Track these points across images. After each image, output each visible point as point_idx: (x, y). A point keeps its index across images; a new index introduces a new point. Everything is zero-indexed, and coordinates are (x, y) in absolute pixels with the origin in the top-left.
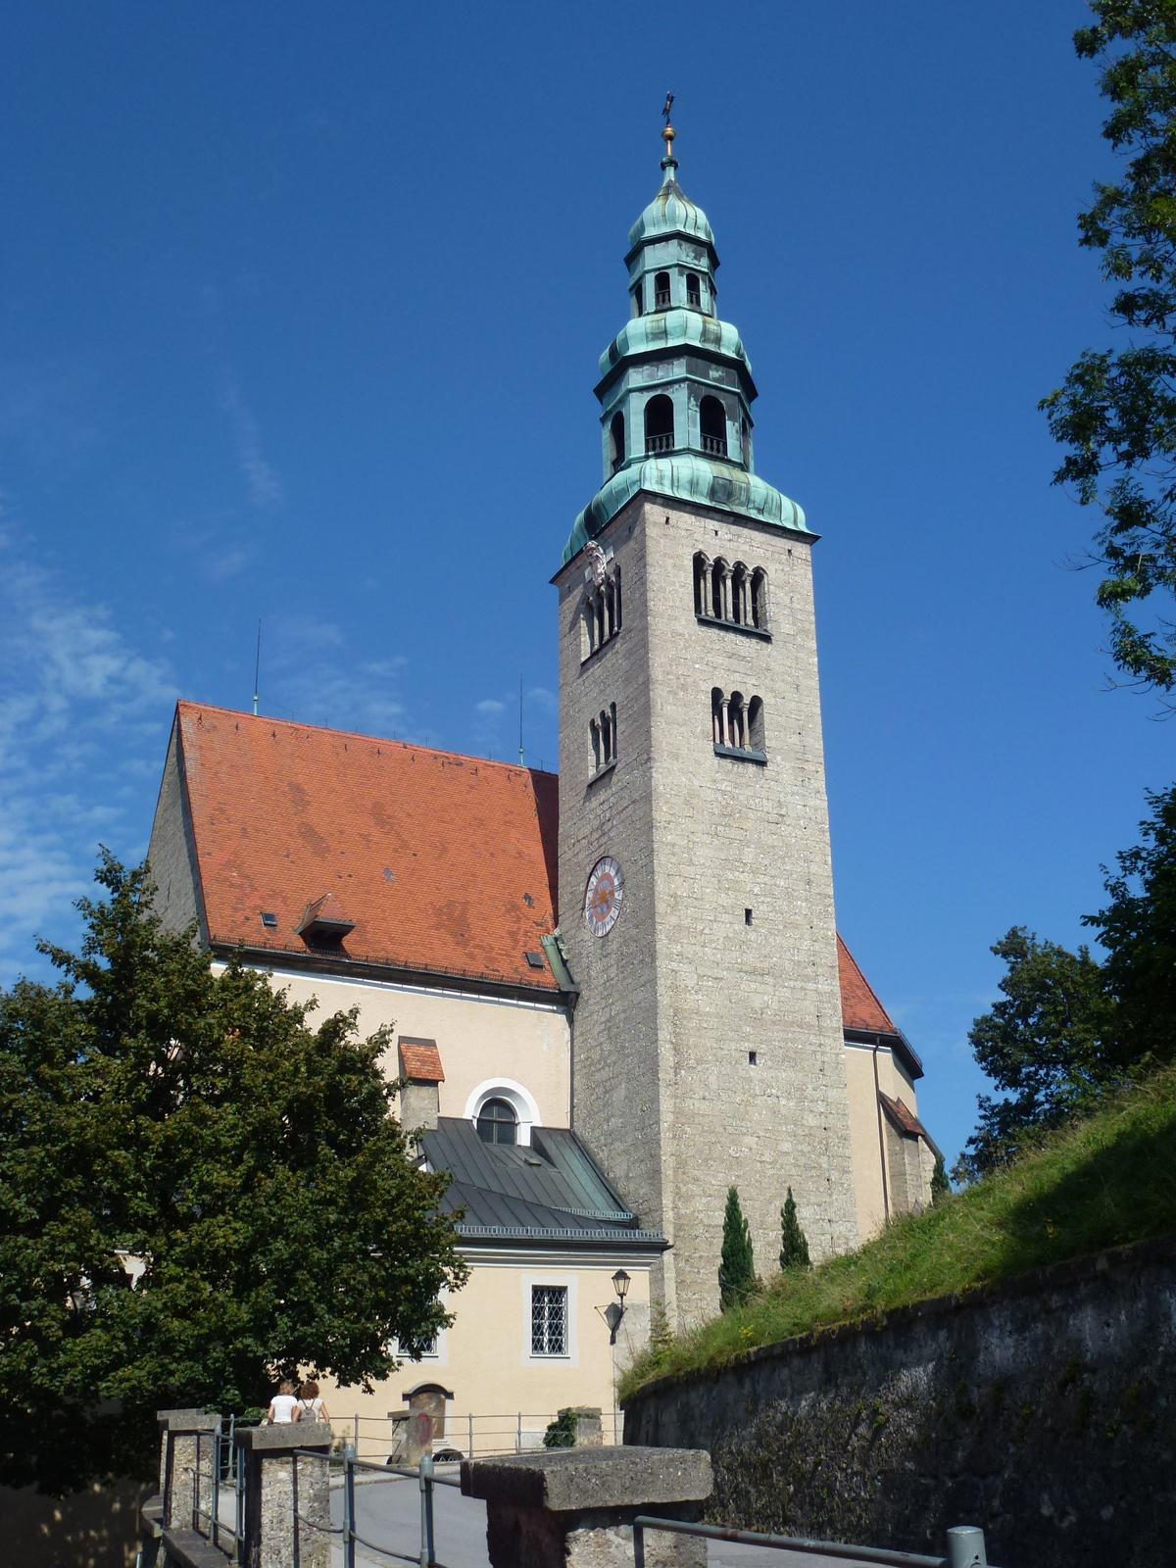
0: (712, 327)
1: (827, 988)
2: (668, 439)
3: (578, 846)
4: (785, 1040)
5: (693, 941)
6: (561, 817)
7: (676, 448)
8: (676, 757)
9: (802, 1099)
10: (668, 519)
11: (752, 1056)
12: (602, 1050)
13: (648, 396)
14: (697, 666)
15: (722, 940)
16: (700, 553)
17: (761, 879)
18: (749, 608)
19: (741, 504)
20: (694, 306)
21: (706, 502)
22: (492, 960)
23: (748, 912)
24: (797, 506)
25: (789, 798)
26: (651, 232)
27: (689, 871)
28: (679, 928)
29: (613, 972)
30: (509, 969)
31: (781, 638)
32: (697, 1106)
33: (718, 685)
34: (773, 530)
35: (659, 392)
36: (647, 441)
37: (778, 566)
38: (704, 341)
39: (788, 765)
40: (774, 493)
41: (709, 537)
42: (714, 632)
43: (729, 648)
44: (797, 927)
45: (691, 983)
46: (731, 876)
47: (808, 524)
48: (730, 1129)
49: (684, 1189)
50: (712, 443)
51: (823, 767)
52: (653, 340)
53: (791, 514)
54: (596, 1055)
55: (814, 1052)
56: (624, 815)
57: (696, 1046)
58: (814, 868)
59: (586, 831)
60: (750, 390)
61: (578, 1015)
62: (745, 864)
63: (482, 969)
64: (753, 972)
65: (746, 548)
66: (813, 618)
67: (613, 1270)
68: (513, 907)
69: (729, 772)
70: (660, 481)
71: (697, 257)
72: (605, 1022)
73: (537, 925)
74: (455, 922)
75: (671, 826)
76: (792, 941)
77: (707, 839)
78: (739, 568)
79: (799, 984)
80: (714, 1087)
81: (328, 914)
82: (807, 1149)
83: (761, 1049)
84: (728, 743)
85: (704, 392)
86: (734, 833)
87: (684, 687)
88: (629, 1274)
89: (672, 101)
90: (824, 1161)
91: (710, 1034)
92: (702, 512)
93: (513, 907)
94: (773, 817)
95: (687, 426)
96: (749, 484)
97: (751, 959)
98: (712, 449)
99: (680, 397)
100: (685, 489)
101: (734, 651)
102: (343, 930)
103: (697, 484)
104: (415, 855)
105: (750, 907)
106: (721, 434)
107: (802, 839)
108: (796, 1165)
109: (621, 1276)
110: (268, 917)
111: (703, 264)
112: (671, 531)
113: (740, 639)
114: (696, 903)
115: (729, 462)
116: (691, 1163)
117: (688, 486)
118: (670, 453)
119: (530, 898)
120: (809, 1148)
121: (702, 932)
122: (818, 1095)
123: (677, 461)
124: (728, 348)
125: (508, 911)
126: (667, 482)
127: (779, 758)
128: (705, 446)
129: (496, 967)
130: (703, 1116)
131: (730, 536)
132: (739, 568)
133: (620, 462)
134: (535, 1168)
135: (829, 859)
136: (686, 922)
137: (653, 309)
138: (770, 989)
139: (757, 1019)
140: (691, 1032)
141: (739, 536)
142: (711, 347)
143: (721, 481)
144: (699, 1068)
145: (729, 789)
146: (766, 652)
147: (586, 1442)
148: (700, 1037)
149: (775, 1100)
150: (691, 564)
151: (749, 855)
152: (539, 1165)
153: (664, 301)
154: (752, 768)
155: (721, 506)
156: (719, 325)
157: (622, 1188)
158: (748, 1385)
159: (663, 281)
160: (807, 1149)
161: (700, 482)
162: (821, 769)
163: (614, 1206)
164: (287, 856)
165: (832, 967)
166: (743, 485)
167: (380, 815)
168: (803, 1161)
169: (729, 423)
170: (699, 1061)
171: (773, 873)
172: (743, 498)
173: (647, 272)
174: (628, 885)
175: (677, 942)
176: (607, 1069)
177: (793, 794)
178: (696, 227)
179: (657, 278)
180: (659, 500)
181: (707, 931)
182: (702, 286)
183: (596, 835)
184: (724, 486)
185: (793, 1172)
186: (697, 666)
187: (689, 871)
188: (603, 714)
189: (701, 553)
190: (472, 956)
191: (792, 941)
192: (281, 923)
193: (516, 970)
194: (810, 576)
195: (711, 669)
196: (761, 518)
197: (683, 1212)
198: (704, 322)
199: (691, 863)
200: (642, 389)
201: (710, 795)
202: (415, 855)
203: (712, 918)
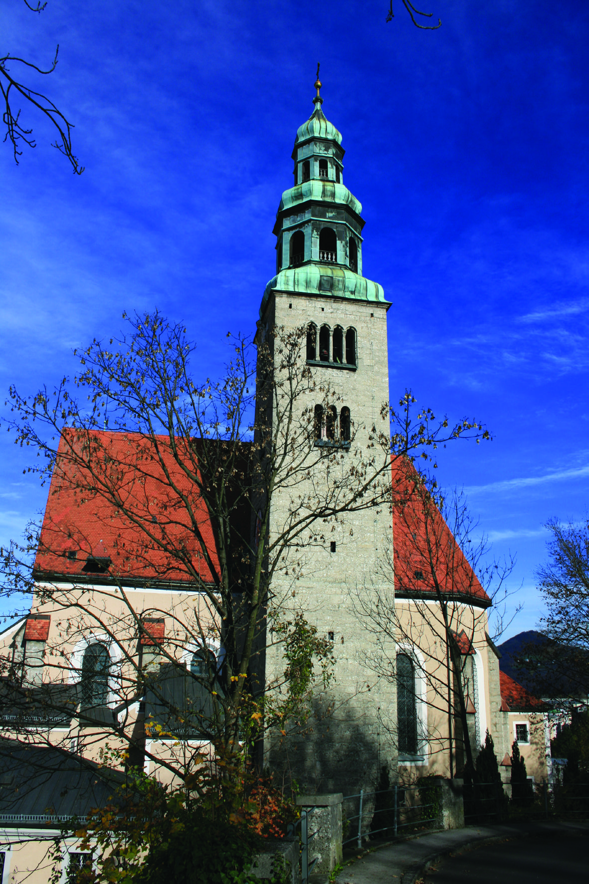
21: (317, 292)
26: (302, 139)
44: (366, 549)
47: (385, 297)
53: (374, 290)
65: (343, 316)
70: (287, 283)
71: (327, 149)
78: (338, 329)
95: (313, 248)
97: (333, 573)
102: (107, 563)
106: (334, 250)
112: (293, 312)
117: (304, 284)
126: (291, 283)
132: (338, 329)
142: (328, 199)
146: (352, 379)
147: (369, 790)
149: (344, 661)
155: (327, 291)
169: (338, 242)
172: (341, 286)
189: (325, 324)
191: (362, 559)
198: (324, 186)
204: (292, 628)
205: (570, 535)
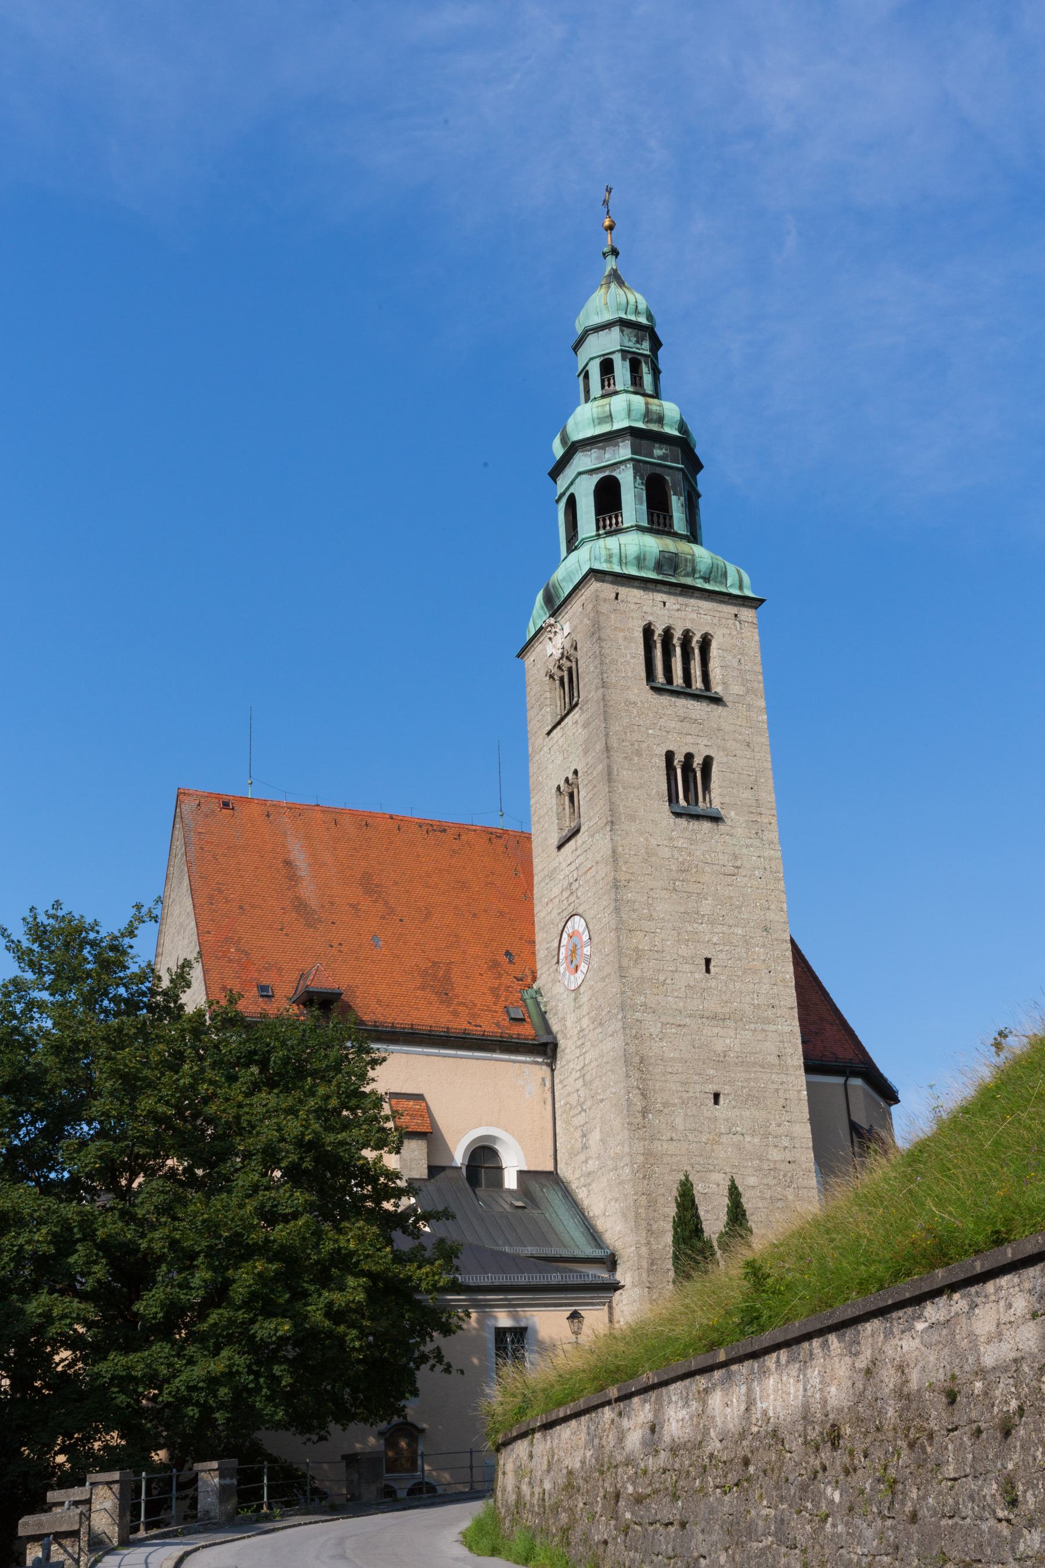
0: (654, 408)
1: (787, 1029)
2: (617, 518)
3: (550, 905)
4: (748, 1080)
5: (655, 991)
6: (535, 878)
7: (625, 526)
8: (632, 818)
9: (765, 1136)
10: (617, 594)
11: (716, 1097)
12: (579, 1096)
13: (596, 478)
14: (650, 732)
15: (683, 989)
16: (650, 624)
17: (719, 929)
18: (699, 673)
19: (687, 575)
20: (638, 389)
21: (653, 575)
22: (474, 1016)
23: (708, 961)
24: (743, 572)
25: (744, 851)
27: (647, 925)
28: (642, 980)
29: (585, 1022)
30: (488, 1026)
31: (731, 699)
32: (665, 1147)
33: (671, 748)
34: (718, 597)
35: (607, 473)
36: (597, 521)
37: (726, 631)
38: (647, 422)
39: (742, 819)
40: (720, 560)
41: (658, 608)
42: (665, 700)
43: (681, 713)
45: (655, 1030)
46: (690, 928)
48: (698, 1167)
49: (655, 1227)
50: (658, 517)
51: (775, 818)
52: (599, 424)
54: (573, 1100)
55: (777, 1090)
56: (590, 874)
57: (662, 1090)
58: (771, 916)
59: (556, 891)
60: (694, 465)
61: (559, 1064)
62: (703, 916)
63: (465, 1026)
64: (715, 1017)
65: (694, 616)
66: (761, 677)
67: (567, 1312)
68: (495, 965)
69: (686, 829)
72: (580, 1070)
73: (518, 980)
74: (439, 983)
75: (632, 884)
76: (751, 986)
77: (665, 894)
79: (759, 1026)
80: (681, 1127)
81: (324, 982)
82: (772, 1182)
83: (725, 1090)
84: (682, 802)
85: (649, 470)
86: (693, 888)
87: (638, 753)
88: (583, 1313)
89: (610, 192)
90: (790, 1193)
91: (675, 1078)
92: (650, 586)
93: (495, 965)
94: (730, 869)
95: (632, 505)
96: (693, 555)
97: (712, 1005)
98: (659, 525)
99: (626, 477)
100: (632, 565)
101: (686, 715)
103: (644, 559)
104: (401, 920)
105: (709, 956)
107: (758, 888)
108: (763, 1198)
109: (575, 1316)
110: (263, 988)
111: (645, 348)
112: (622, 607)
113: (691, 703)
114: (657, 956)
115: (675, 535)
116: (661, 1200)
117: (635, 562)
118: (618, 531)
119: (511, 954)
120: (775, 1182)
121: (664, 983)
122: (780, 1131)
123: (623, 538)
124: (671, 426)
125: (490, 968)
126: (615, 560)
127: (732, 813)
128: (651, 521)
129: (478, 1022)
130: (671, 1156)
131: (677, 607)
133: (572, 544)
134: (520, 1211)
135: (785, 906)
136: (648, 974)
137: (599, 393)
138: (732, 1033)
139: (721, 1061)
140: (657, 1077)
141: (686, 605)
142: (654, 427)
143: (666, 555)
144: (666, 1111)
145: (685, 845)
146: (716, 714)
148: (666, 1081)
149: (740, 1138)
150: (641, 635)
151: (706, 906)
152: (524, 1208)
153: (609, 385)
154: (706, 825)
156: (661, 406)
157: (601, 1224)
158: (549, 1442)
159: (607, 367)
160: (772, 1182)
161: (648, 557)
162: (774, 821)
163: (593, 1243)
164: (282, 930)
165: (792, 1008)
166: (689, 557)
167: (369, 885)
168: (768, 1194)
170: (665, 1105)
171: (731, 922)
172: (689, 569)
173: (592, 359)
174: (595, 939)
175: (640, 993)
176: (583, 1114)
177: (747, 846)
178: (637, 312)
179: (602, 364)
180: (608, 578)
181: (668, 981)
182: (645, 369)
183: (566, 894)
184: (670, 559)
185: (760, 1205)
186: (650, 732)
187: (647, 925)
188: (567, 780)
190: (455, 1014)
192: (279, 993)
193: (498, 1025)
194: (757, 638)
195: (665, 734)
196: (707, 586)
197: (655, 1247)
198: (647, 404)
199: (651, 918)
200: (591, 472)
201: (665, 852)
202: (401, 920)
203: (673, 969)
204: (391, 1256)
205: (488, 1414)
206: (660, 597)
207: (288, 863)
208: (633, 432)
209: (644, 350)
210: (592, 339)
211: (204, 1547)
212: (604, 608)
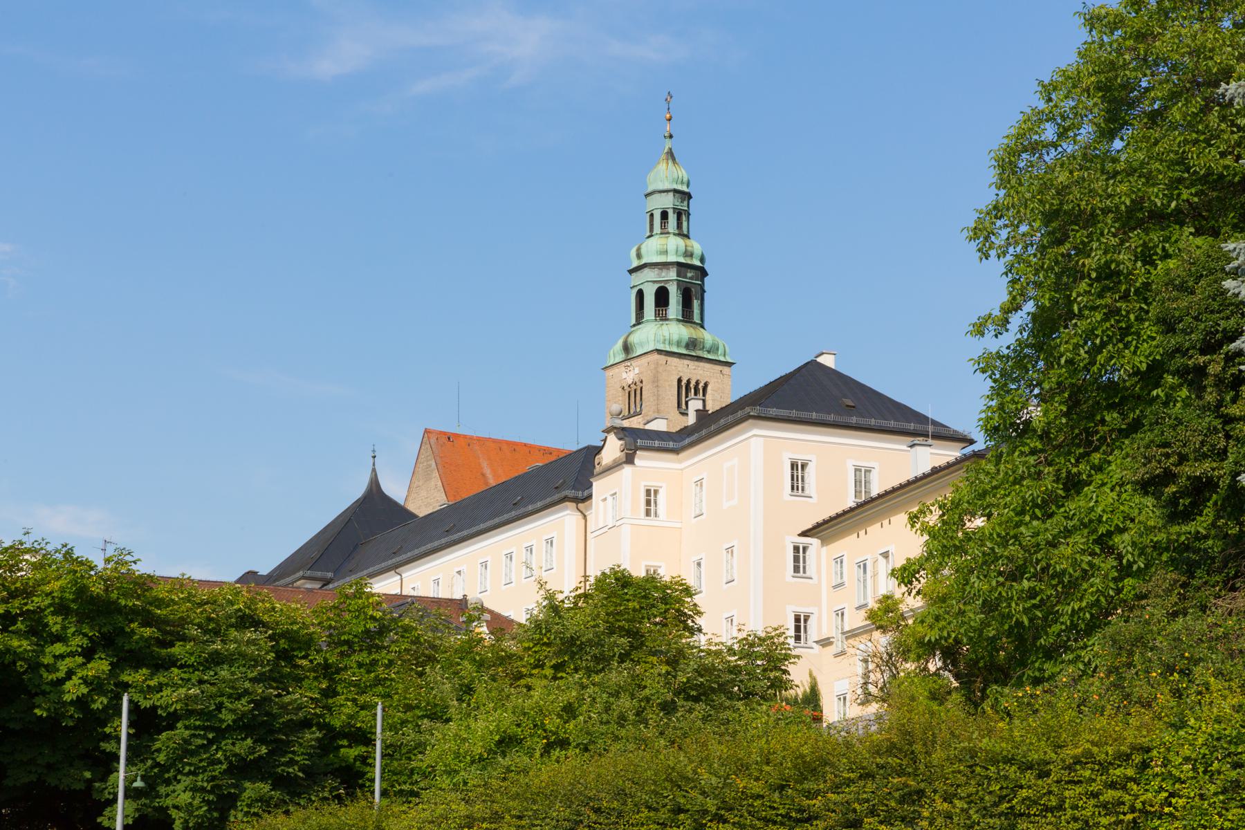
13: (657, 286)
21: (684, 352)
95: (674, 308)
99: (673, 290)
200: (654, 282)
206: (686, 362)
207: (483, 475)
208: (679, 264)
209: (679, 215)
210: (646, 270)
211: (661, 192)
212: (660, 369)
